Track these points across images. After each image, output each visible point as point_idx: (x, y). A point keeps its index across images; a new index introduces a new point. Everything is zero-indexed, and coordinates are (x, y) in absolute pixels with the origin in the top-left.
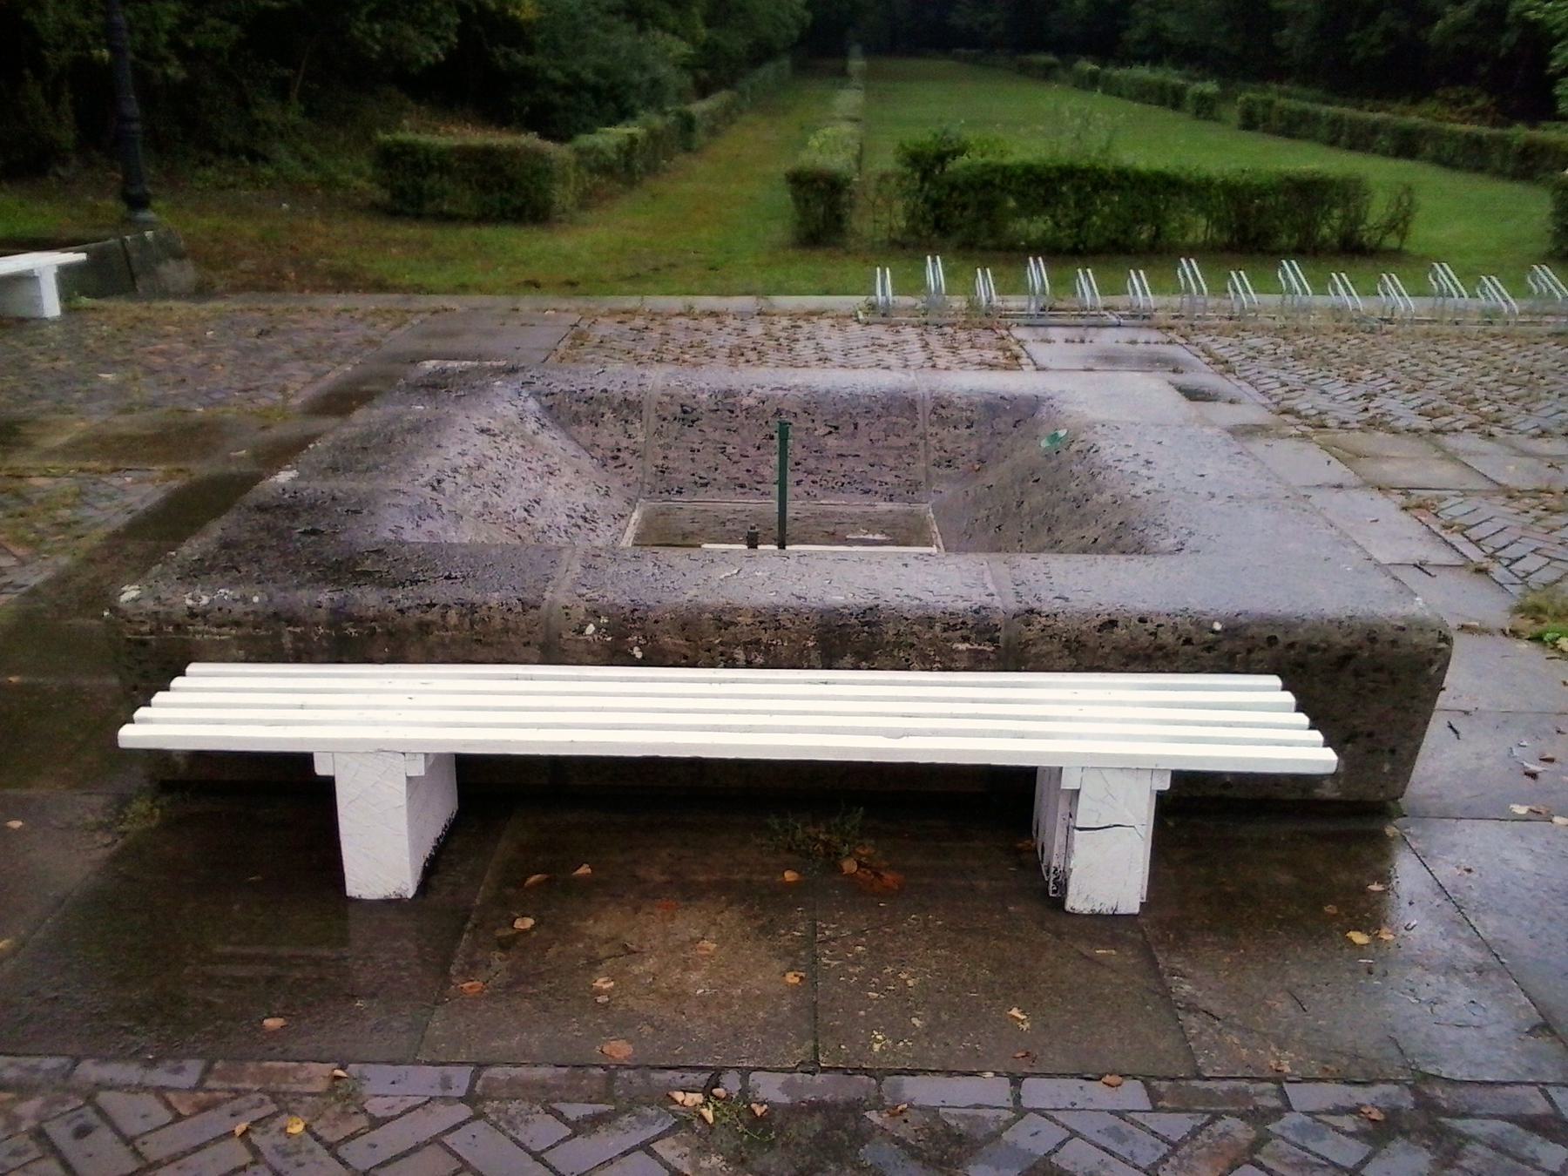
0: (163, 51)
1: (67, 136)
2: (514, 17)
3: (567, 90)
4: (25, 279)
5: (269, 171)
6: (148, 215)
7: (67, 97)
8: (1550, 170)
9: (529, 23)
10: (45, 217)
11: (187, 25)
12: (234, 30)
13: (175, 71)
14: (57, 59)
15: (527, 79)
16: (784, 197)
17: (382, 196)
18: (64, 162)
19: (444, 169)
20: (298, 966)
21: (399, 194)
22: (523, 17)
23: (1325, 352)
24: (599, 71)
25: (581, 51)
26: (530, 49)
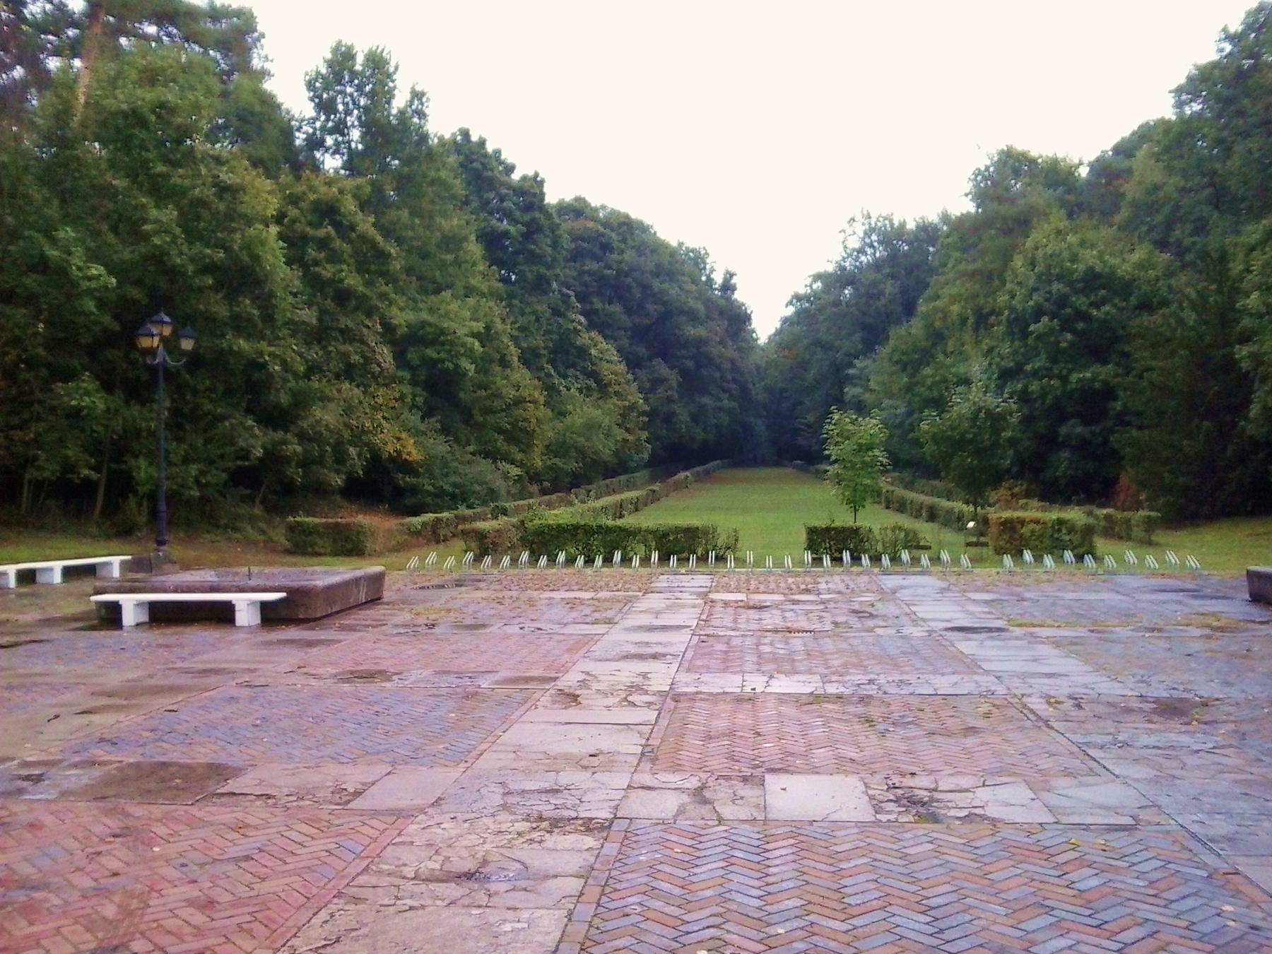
0: (190, 484)
1: (142, 519)
2: (406, 460)
3: (437, 496)
4: (51, 569)
5: (238, 535)
6: (162, 548)
7: (145, 504)
8: (237, 255)
9: (417, 463)
10: (127, 547)
11: (203, 473)
12: (224, 475)
13: (196, 493)
14: (142, 490)
15: (414, 490)
16: (1244, 582)
17: (288, 545)
18: (140, 531)
19: (320, 535)
20: (1237, 893)
21: (296, 545)
22: (411, 459)
23: (156, 877)
24: (455, 485)
25: (447, 475)
26: (417, 474)
